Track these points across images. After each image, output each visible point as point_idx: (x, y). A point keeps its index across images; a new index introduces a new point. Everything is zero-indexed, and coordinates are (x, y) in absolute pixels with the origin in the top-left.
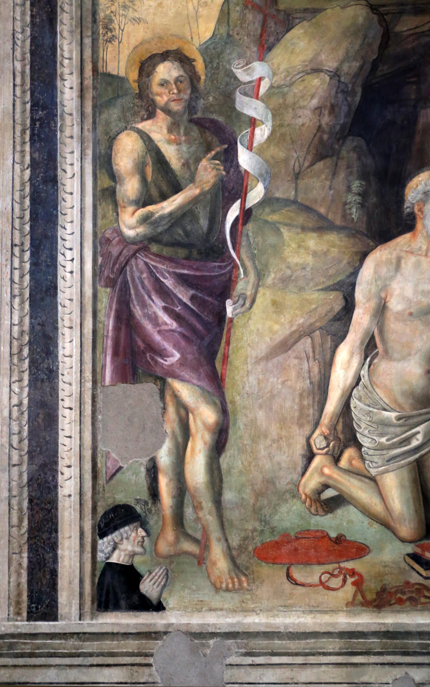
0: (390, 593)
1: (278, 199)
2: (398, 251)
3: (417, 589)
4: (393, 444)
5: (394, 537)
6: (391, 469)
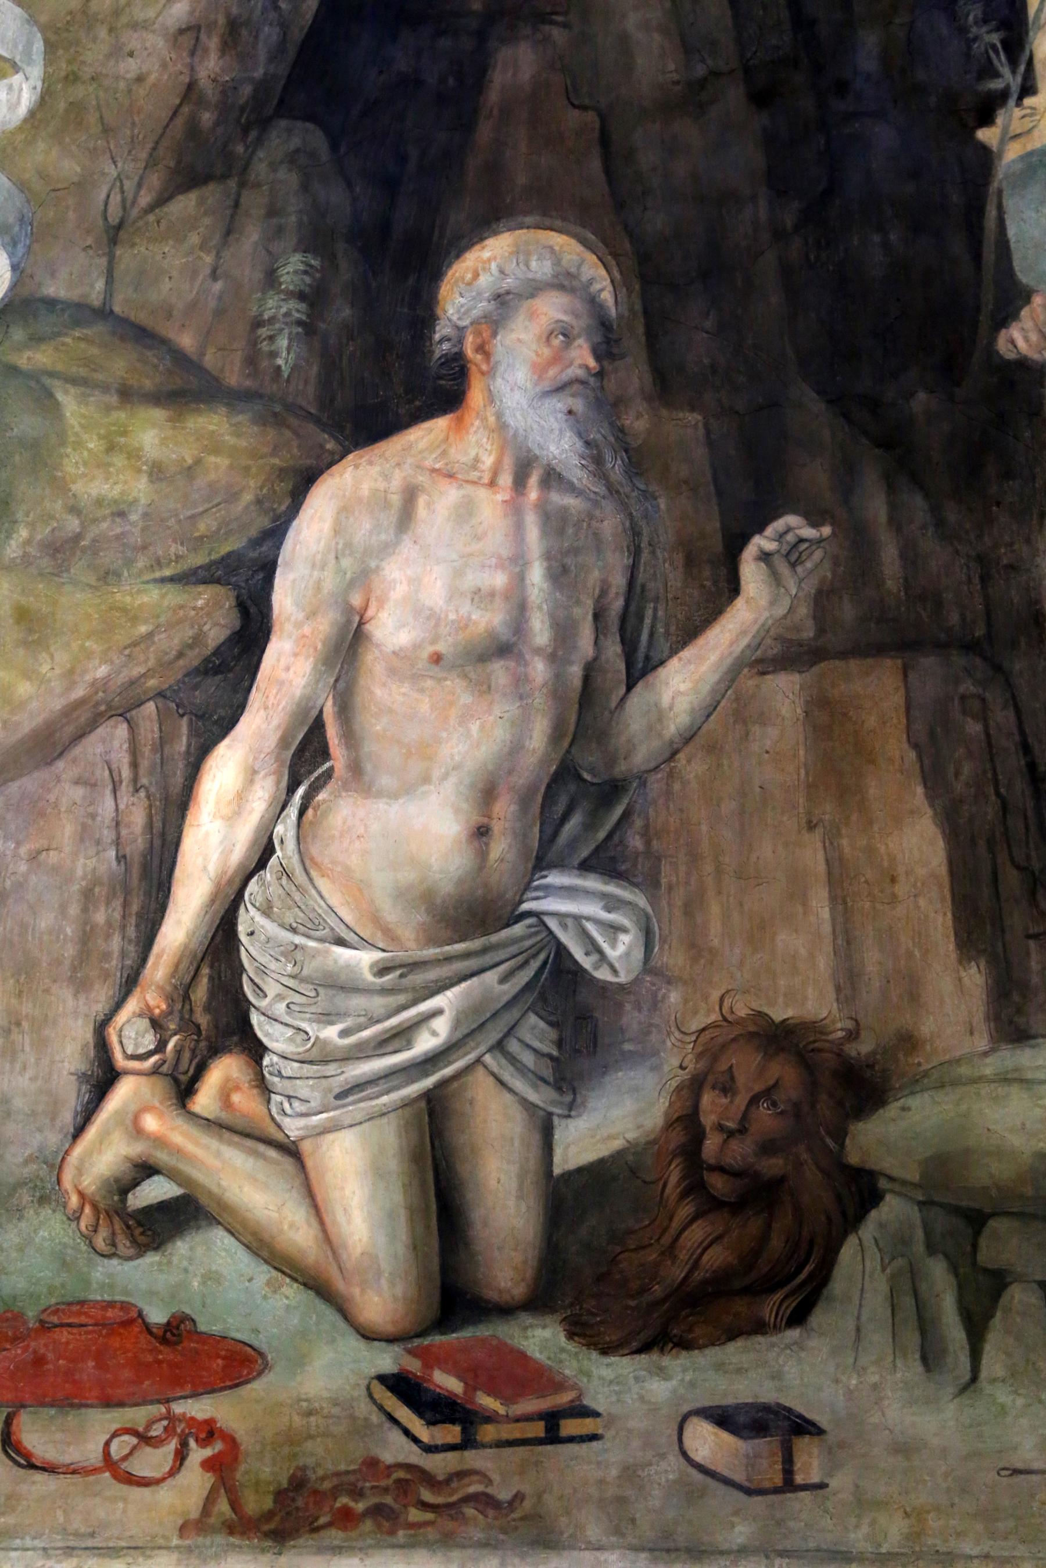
0: (315, 1492)
1: (51, 303)
2: (408, 469)
3: (399, 1481)
4: (360, 1046)
5: (342, 1324)
6: (348, 1121)
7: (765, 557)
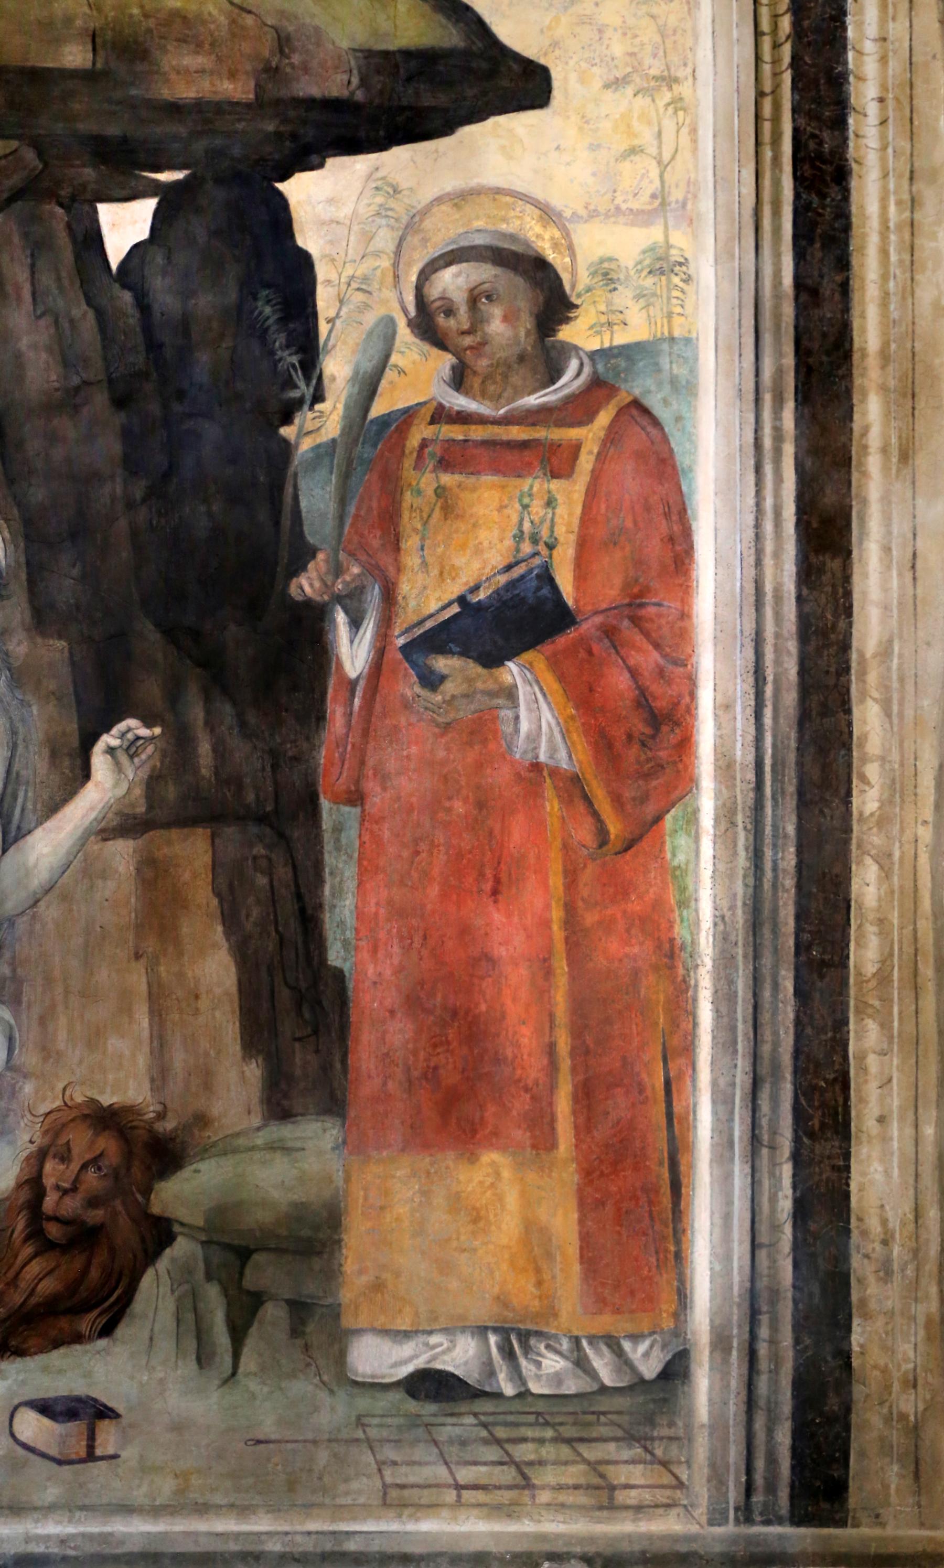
7: (111, 750)
